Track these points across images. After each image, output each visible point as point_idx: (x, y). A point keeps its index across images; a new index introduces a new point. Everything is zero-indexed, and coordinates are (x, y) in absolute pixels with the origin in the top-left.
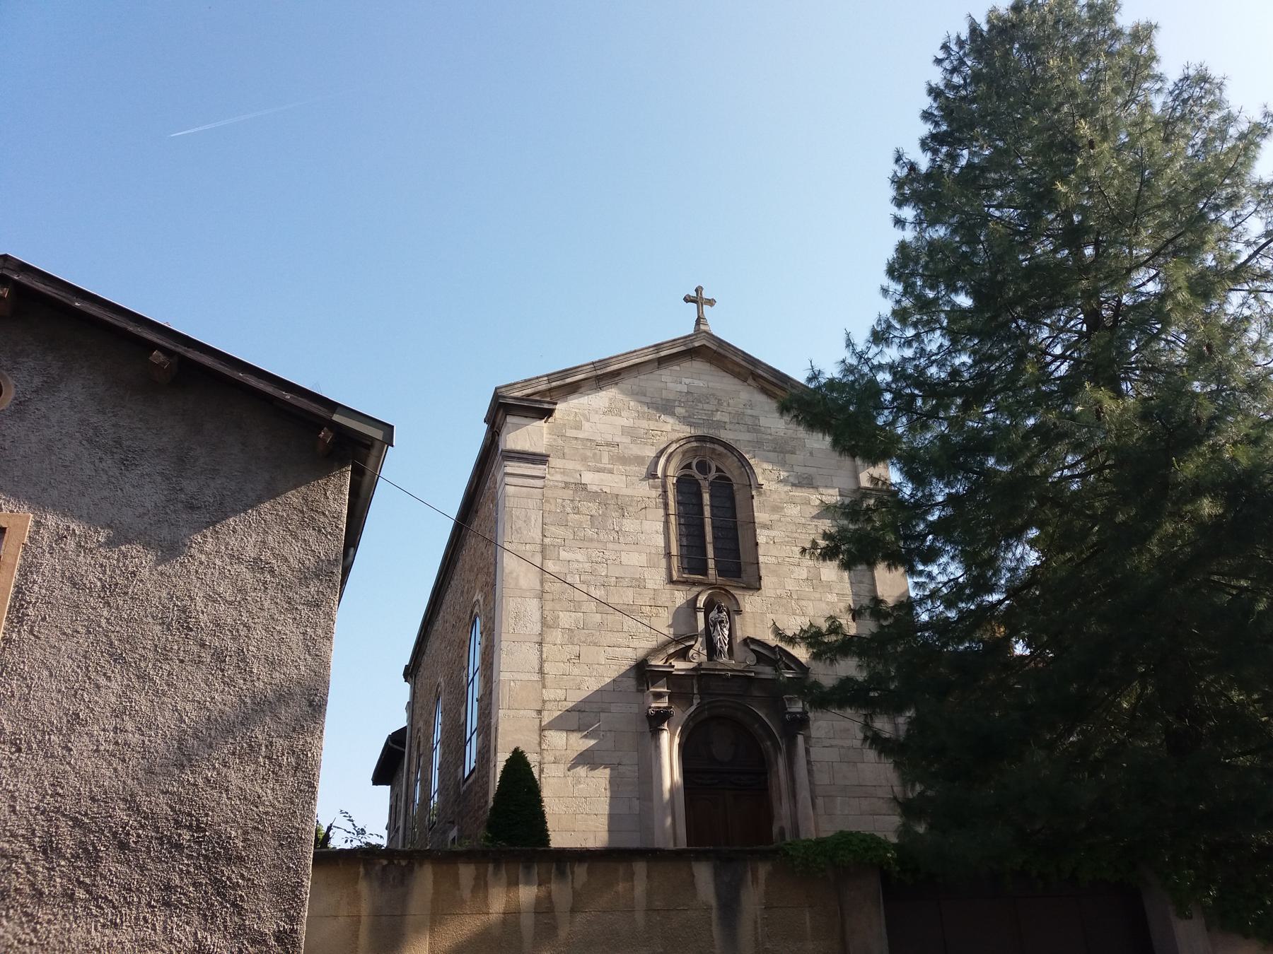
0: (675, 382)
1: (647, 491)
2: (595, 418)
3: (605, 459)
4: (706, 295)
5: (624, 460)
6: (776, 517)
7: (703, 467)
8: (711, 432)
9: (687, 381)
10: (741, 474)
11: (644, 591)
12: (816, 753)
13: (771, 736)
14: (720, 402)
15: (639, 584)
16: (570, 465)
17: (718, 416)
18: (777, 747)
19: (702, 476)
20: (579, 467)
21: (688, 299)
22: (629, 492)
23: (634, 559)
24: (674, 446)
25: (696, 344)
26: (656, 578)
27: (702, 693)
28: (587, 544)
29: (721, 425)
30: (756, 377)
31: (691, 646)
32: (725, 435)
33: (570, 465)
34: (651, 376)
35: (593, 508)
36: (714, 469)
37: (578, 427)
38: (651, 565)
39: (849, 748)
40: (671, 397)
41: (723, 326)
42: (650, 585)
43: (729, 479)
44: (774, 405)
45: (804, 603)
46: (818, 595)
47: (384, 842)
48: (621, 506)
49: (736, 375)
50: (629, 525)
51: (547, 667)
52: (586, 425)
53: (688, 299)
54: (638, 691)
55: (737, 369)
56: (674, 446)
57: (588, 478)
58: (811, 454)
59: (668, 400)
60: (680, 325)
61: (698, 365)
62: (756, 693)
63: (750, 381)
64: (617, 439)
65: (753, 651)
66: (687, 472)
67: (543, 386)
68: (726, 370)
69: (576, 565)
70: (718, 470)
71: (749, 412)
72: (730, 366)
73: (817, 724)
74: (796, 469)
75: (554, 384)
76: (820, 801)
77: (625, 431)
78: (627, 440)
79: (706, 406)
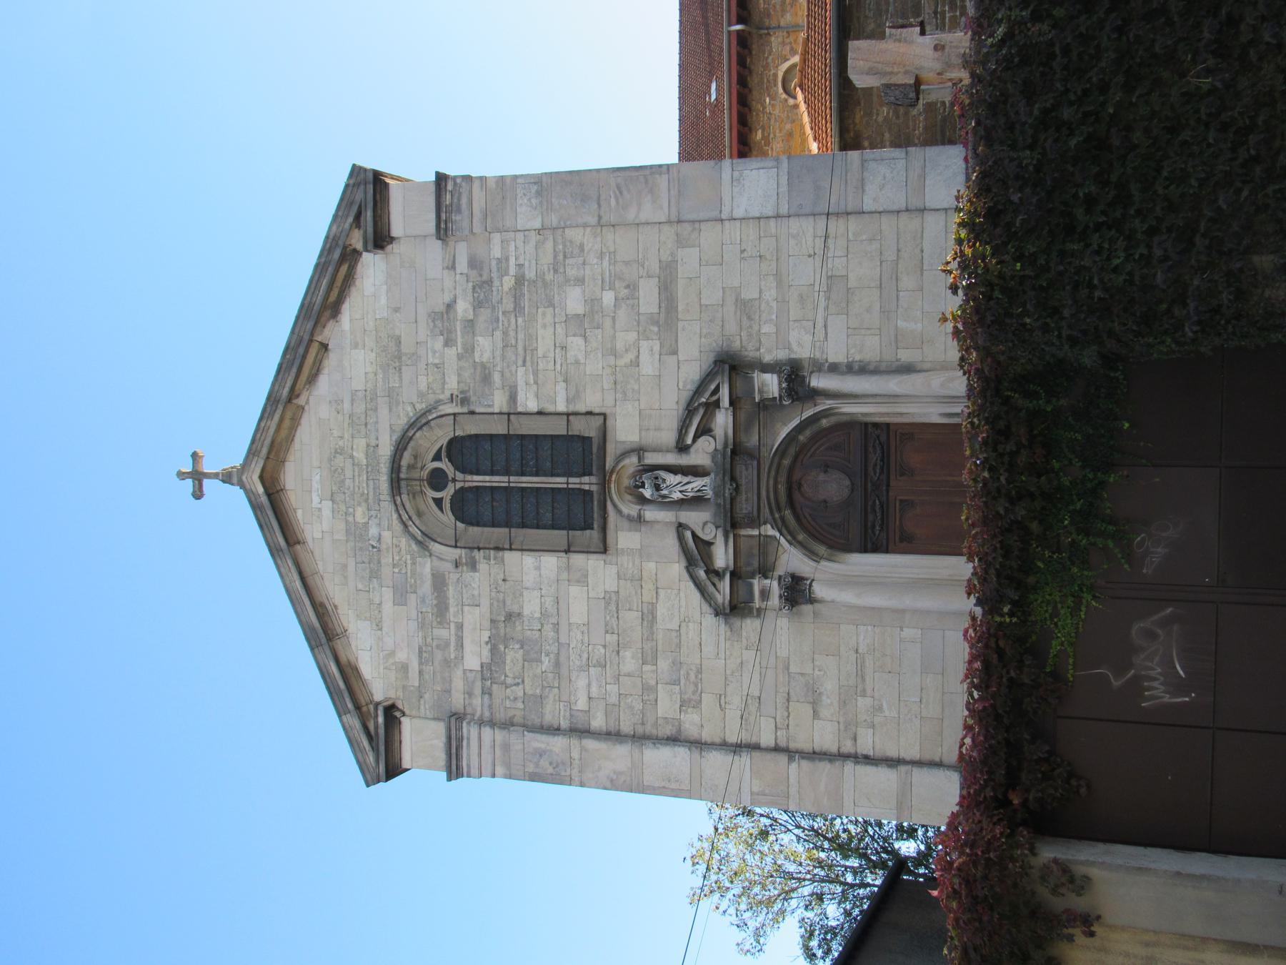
0: (320, 517)
1: (481, 580)
2: (389, 642)
3: (442, 633)
4: (188, 468)
5: (441, 609)
6: (496, 377)
7: (437, 479)
8: (384, 468)
9: (316, 499)
10: (439, 426)
11: (622, 593)
12: (836, 354)
13: (815, 418)
14: (339, 451)
15: (612, 602)
16: (458, 684)
17: (360, 455)
18: (825, 413)
19: (451, 485)
20: (459, 673)
21: (198, 494)
22: (485, 603)
23: (578, 606)
24: (413, 529)
25: (261, 490)
26: (600, 573)
27: (755, 522)
28: (564, 671)
29: (372, 449)
30: (293, 395)
31: (694, 535)
32: (386, 450)
33: (458, 684)
34: (317, 553)
35: (513, 656)
36: (437, 464)
37: (404, 668)
38: (583, 580)
39: (828, 298)
40: (342, 526)
41: (230, 444)
42: (611, 585)
43: (451, 442)
44: (331, 324)
45: (620, 345)
46: (608, 323)
47: (961, 568)
48: (505, 621)
49: (296, 422)
50: (531, 606)
51: (732, 739)
52: (402, 656)
53: (198, 494)
54: (758, 616)
55: (287, 423)
56: (413, 529)
57: (473, 660)
58: (397, 310)
59: (348, 532)
60: (232, 509)
61: (290, 478)
62: (754, 439)
63: (301, 401)
64: (414, 614)
65: (694, 440)
66: (447, 505)
67: (355, 722)
68: (290, 438)
69: (594, 689)
70: (437, 457)
71: (347, 405)
72: (283, 433)
73: (794, 346)
74: (422, 337)
75: (350, 705)
76: (905, 356)
77: (401, 596)
78: (412, 599)
79: (349, 473)
